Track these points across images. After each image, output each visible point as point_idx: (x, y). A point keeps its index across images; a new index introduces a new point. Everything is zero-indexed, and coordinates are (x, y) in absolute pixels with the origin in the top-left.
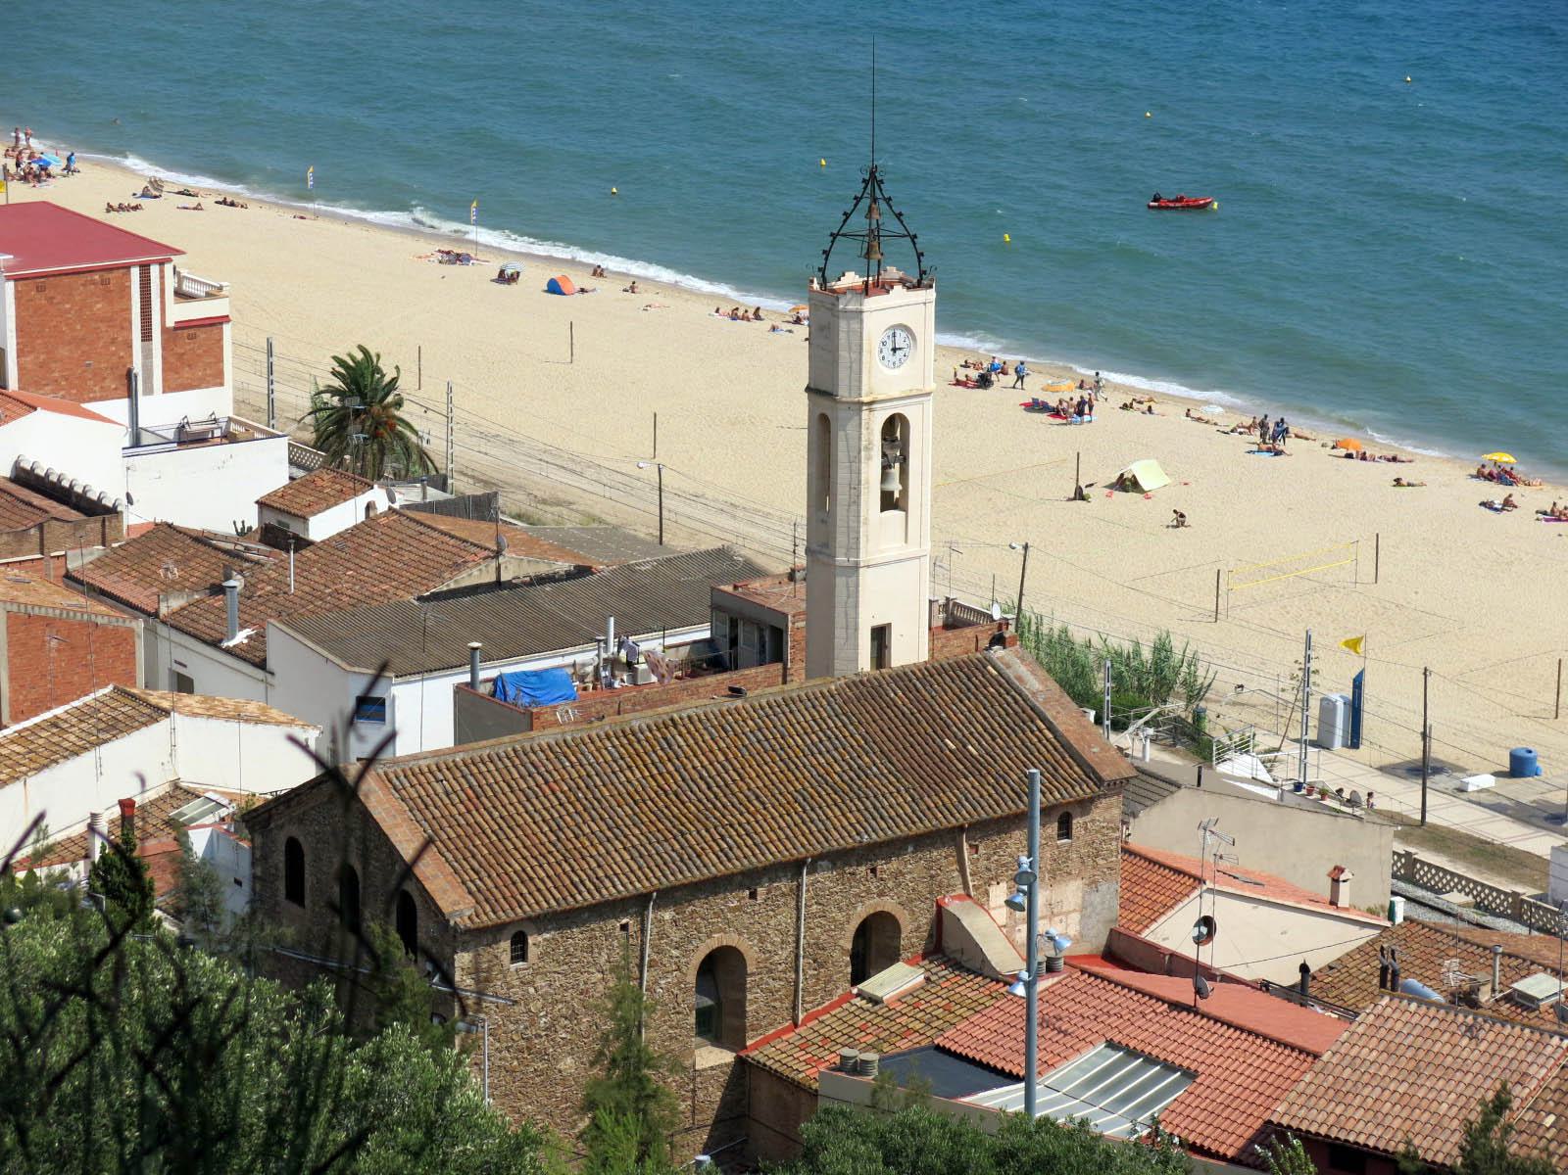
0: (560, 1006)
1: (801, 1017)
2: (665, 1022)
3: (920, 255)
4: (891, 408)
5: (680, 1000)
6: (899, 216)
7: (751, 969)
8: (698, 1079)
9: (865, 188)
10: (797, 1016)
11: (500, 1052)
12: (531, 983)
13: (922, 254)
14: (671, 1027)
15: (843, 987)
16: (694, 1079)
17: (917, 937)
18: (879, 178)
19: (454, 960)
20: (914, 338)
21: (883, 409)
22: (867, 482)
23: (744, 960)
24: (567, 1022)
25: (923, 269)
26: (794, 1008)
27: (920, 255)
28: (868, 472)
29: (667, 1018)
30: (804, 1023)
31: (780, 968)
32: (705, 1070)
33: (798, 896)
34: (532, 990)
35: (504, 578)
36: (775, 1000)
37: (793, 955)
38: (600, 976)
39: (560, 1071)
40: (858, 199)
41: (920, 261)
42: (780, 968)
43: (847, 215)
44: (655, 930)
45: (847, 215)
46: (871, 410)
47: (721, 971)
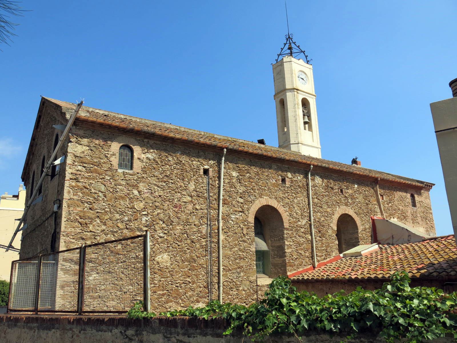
0: (159, 211)
2: (236, 245)
3: (306, 57)
4: (305, 95)
5: (245, 232)
8: (259, 292)
9: (287, 41)
11: (106, 234)
12: (136, 187)
13: (307, 56)
14: (240, 250)
15: (335, 253)
16: (257, 292)
17: (366, 235)
18: (291, 37)
19: (68, 146)
20: (308, 78)
21: (301, 94)
24: (164, 225)
25: (308, 60)
26: (312, 257)
27: (306, 57)
28: (298, 112)
31: (302, 230)
32: (263, 286)
33: (307, 190)
34: (136, 192)
36: (302, 249)
37: (308, 225)
38: (189, 199)
39: (158, 263)
40: (285, 44)
41: (307, 58)
42: (302, 230)
43: (282, 49)
44: (227, 181)
45: (282, 49)
46: (298, 93)
47: (266, 221)
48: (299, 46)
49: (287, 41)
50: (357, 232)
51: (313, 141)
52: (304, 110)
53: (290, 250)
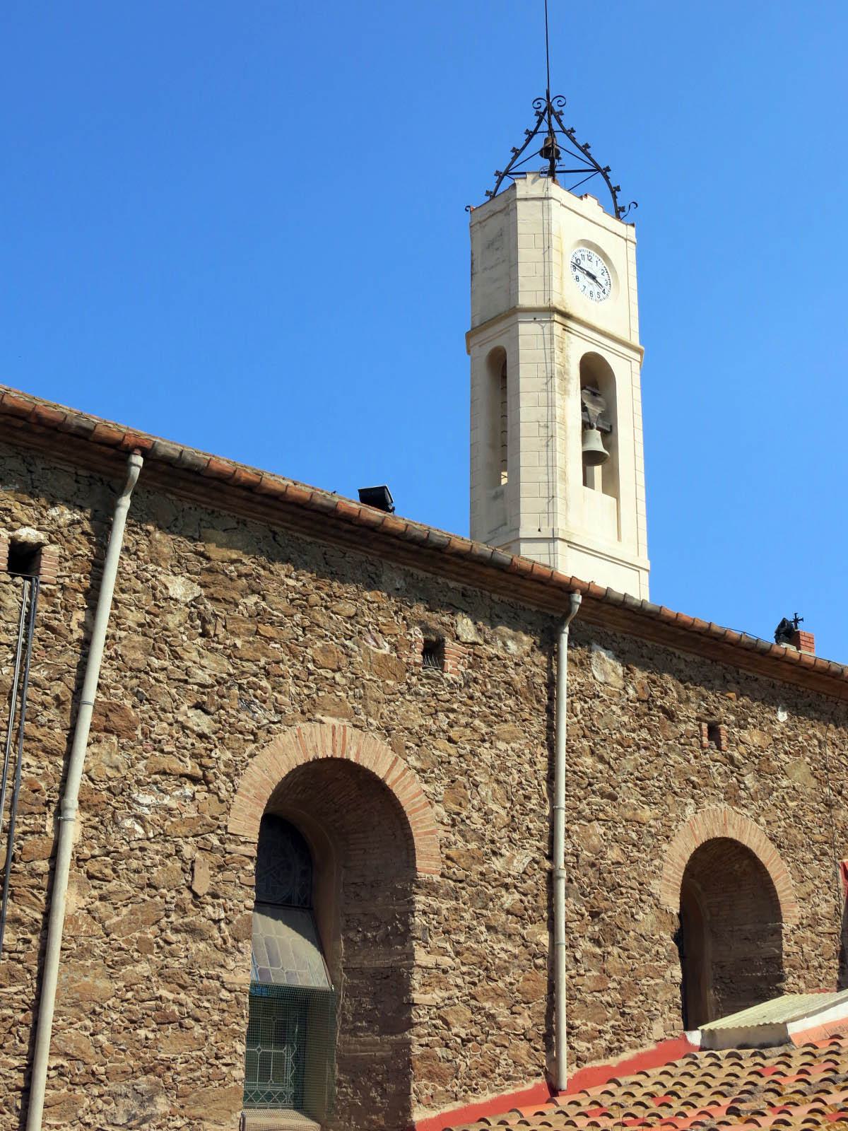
1: (567, 1073)
3: (614, 191)
4: (598, 344)
6: (585, 149)
7: (428, 865)
9: (539, 122)
10: (557, 1076)
13: (618, 189)
14: (164, 975)
15: (664, 1025)
18: (557, 109)
22: (563, 423)
23: (409, 837)
27: (614, 191)
29: (150, 932)
30: (581, 1084)
31: (509, 899)
35: (21, 1084)
40: (531, 135)
42: (509, 899)
45: (517, 153)
46: (566, 329)
48: (587, 146)
49: (539, 122)
50: (777, 931)
51: (619, 538)
52: (588, 405)
53: (436, 996)
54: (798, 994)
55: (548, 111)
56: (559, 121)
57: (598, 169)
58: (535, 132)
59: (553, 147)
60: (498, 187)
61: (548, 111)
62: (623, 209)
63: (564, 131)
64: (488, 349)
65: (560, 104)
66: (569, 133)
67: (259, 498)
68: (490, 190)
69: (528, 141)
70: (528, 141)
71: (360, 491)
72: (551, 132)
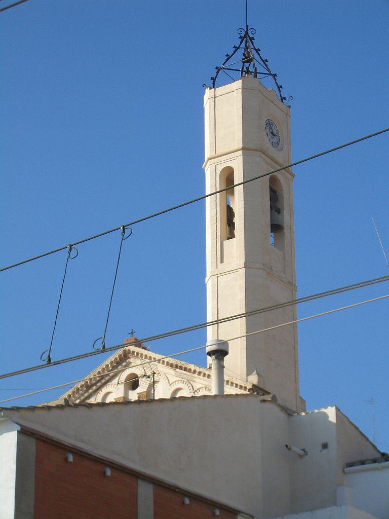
6: (265, 61)
9: (241, 42)
40: (237, 48)
45: (229, 57)
49: (241, 42)
54: (152, 357)
55: (246, 37)
56: (253, 43)
57: (271, 74)
58: (239, 48)
59: (246, 59)
60: (241, 44)
61: (246, 37)
62: (284, 98)
63: (255, 49)
64: (220, 168)
65: (252, 32)
66: (257, 51)
67: (35, 436)
68: (213, 77)
69: (235, 52)
70: (235, 52)
71: (235, 237)
72: (246, 48)
